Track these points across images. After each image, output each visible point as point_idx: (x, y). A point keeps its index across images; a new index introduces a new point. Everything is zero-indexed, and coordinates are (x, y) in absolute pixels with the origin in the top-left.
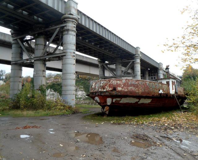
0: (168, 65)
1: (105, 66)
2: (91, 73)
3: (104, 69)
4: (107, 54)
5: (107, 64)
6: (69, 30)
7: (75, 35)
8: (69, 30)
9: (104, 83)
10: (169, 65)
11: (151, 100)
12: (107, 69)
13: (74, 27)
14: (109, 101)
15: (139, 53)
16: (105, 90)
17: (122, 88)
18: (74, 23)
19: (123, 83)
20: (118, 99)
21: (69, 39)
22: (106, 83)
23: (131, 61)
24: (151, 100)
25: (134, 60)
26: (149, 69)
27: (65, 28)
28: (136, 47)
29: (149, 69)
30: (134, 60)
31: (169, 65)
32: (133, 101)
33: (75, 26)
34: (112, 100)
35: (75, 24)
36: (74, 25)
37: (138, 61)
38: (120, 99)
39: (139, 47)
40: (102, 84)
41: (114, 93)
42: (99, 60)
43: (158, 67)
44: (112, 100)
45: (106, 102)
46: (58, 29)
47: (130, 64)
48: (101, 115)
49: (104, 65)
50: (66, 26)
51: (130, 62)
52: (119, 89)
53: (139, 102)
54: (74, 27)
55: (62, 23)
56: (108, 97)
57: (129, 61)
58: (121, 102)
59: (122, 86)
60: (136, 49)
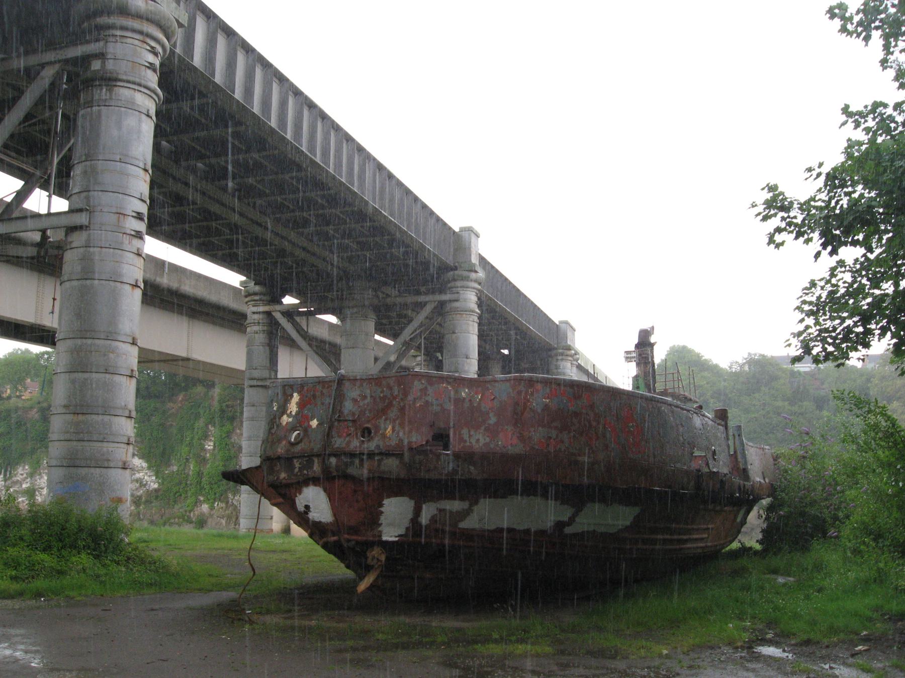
0: (646, 326)
1: (283, 321)
2: (196, 356)
3: (275, 337)
4: (302, 255)
5: (290, 313)
6: (117, 80)
7: (153, 112)
8: (117, 80)
9: (365, 397)
10: (653, 327)
11: (636, 510)
12: (292, 344)
13: (151, 66)
14: (395, 517)
15: (474, 260)
16: (372, 446)
17: (492, 432)
18: (153, 44)
19: (496, 403)
20: (456, 505)
21: (115, 133)
22: (383, 399)
23: (429, 298)
24: (636, 510)
25: (444, 297)
26: (506, 352)
27: (96, 65)
28: (457, 230)
29: (506, 352)
30: (444, 297)
31: (653, 327)
32: (546, 514)
33: (157, 62)
34: (417, 511)
35: (159, 49)
36: (151, 58)
37: (470, 299)
38: (465, 505)
39: (477, 228)
40: (355, 401)
41: (447, 464)
42: (253, 287)
43: (553, 343)
44: (417, 511)
45: (373, 519)
46: (48, 73)
47: (428, 309)
48: (317, 597)
49: (278, 316)
50: (101, 56)
51: (422, 305)
52: (478, 440)
53: (464, 514)
54: (151, 66)
55: (78, 38)
56: (396, 487)
57: (422, 299)
58: (470, 523)
59: (493, 420)
60: (459, 242)
